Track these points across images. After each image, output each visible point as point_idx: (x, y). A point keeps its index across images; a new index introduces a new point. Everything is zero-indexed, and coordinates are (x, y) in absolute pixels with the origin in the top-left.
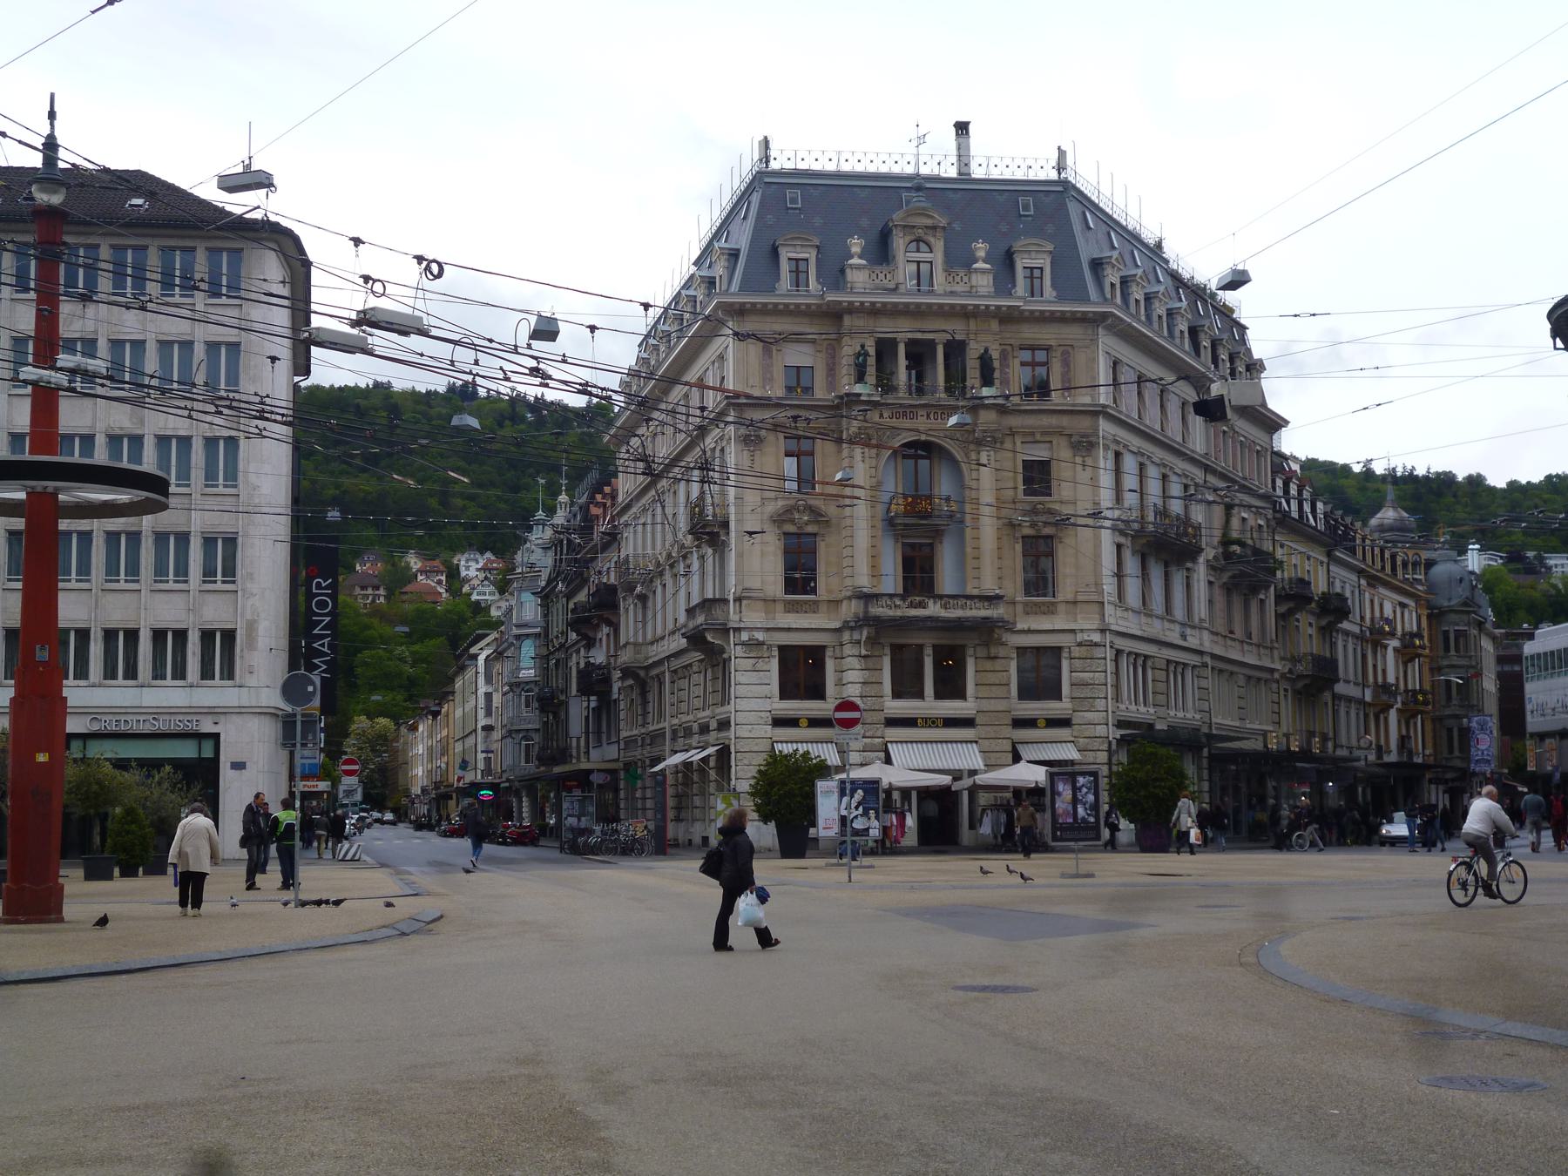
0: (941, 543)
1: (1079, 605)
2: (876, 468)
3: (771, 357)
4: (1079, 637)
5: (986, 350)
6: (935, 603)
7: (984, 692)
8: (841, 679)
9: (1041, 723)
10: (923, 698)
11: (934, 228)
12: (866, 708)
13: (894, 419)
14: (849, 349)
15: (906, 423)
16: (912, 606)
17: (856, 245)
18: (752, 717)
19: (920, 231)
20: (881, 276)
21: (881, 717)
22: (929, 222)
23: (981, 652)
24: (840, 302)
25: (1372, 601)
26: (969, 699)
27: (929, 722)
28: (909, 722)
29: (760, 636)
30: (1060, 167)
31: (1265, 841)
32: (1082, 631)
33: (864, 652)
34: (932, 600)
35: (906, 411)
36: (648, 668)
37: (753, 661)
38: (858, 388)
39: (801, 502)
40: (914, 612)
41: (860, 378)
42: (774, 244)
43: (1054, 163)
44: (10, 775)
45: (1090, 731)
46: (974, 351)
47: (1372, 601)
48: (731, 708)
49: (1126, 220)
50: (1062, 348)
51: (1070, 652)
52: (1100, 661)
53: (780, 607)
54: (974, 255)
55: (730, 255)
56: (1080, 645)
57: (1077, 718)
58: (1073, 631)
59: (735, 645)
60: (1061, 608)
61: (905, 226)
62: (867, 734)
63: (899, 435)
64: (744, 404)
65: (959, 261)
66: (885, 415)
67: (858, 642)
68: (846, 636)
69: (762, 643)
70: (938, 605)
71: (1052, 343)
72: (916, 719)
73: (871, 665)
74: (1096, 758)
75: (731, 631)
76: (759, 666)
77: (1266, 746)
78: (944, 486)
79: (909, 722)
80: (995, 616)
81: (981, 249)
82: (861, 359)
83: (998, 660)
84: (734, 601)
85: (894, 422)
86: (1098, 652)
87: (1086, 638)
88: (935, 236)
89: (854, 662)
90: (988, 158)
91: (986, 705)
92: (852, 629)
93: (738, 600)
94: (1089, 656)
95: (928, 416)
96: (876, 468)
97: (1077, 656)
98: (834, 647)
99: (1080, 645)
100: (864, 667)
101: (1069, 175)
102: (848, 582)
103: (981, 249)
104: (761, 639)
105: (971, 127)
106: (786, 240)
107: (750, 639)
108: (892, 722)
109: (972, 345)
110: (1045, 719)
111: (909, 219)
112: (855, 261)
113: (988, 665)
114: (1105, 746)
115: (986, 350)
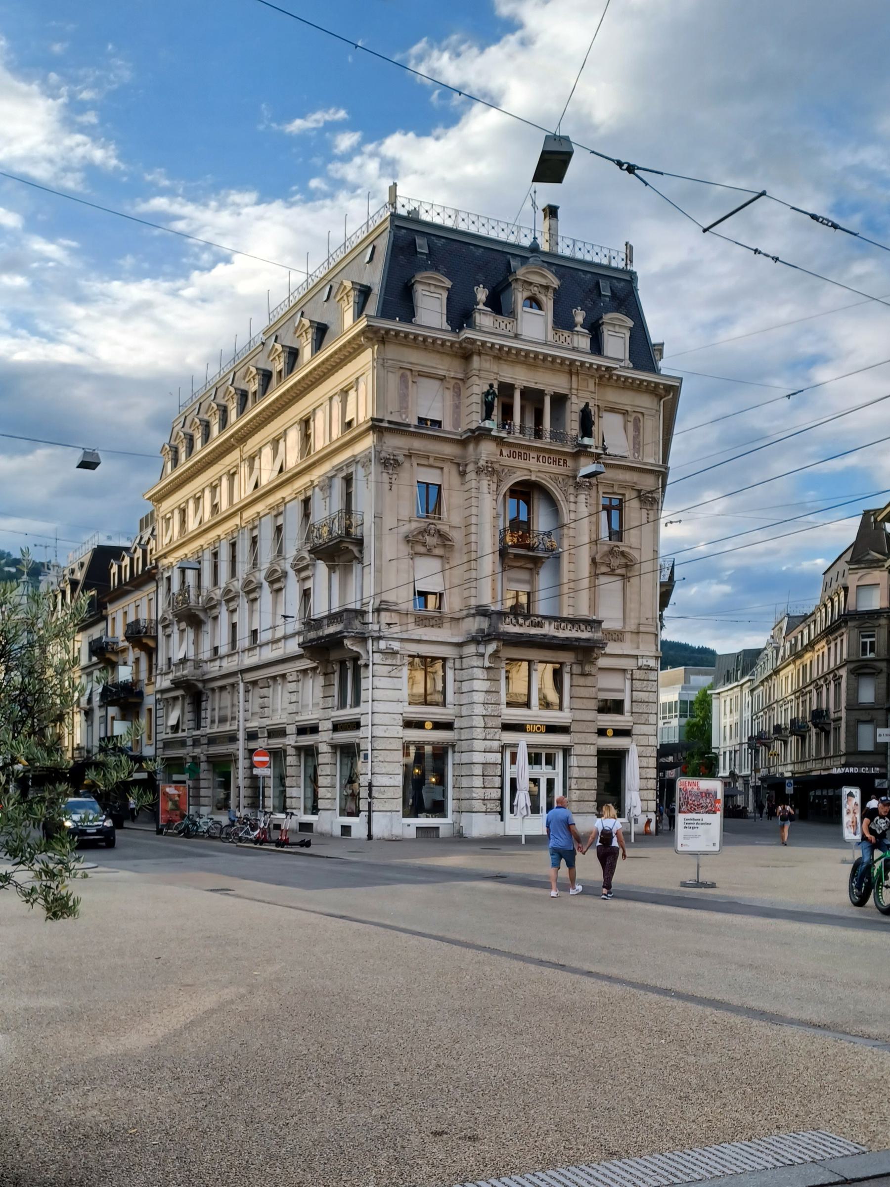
0: (538, 574)
1: (641, 635)
2: (496, 500)
3: (407, 388)
4: (641, 662)
5: (587, 404)
6: (550, 624)
7: (578, 704)
8: (460, 688)
11: (547, 288)
12: (488, 714)
13: (512, 458)
14: (478, 387)
15: (521, 463)
17: (482, 294)
18: (386, 719)
19: (536, 289)
20: (503, 325)
21: (498, 722)
22: (543, 282)
23: (577, 669)
24: (475, 340)
26: (626, 714)
29: (396, 646)
32: (643, 656)
33: (487, 664)
35: (520, 451)
36: (205, 682)
37: (390, 668)
38: (488, 424)
39: (432, 526)
40: (534, 631)
41: (488, 416)
42: (406, 284)
45: (644, 741)
46: (575, 406)
48: (363, 708)
50: (634, 415)
51: (632, 675)
52: (654, 683)
53: (411, 619)
54: (574, 320)
55: (360, 291)
56: (640, 668)
57: (636, 730)
58: (636, 657)
59: (373, 652)
60: (628, 637)
61: (525, 281)
62: (488, 737)
63: (514, 473)
64: (386, 428)
65: (563, 322)
66: (505, 453)
67: (483, 655)
68: (471, 649)
69: (397, 653)
70: (552, 626)
71: (629, 408)
73: (492, 676)
75: (370, 641)
76: (393, 674)
77: (289, 755)
78: (542, 522)
80: (595, 638)
81: (580, 316)
82: (490, 397)
83: (485, 690)
84: (373, 612)
85: (512, 462)
87: (645, 663)
88: (546, 296)
89: (479, 673)
90: (574, 241)
91: (579, 715)
92: (478, 643)
93: (378, 611)
95: (538, 459)
96: (496, 500)
97: (638, 678)
98: (454, 659)
99: (640, 668)
100: (486, 678)
101: (635, 267)
102: (473, 602)
103: (580, 316)
104: (395, 648)
105: (559, 211)
106: (423, 278)
107: (387, 648)
109: (574, 399)
111: (528, 276)
112: (481, 306)
113: (581, 681)
115: (587, 404)
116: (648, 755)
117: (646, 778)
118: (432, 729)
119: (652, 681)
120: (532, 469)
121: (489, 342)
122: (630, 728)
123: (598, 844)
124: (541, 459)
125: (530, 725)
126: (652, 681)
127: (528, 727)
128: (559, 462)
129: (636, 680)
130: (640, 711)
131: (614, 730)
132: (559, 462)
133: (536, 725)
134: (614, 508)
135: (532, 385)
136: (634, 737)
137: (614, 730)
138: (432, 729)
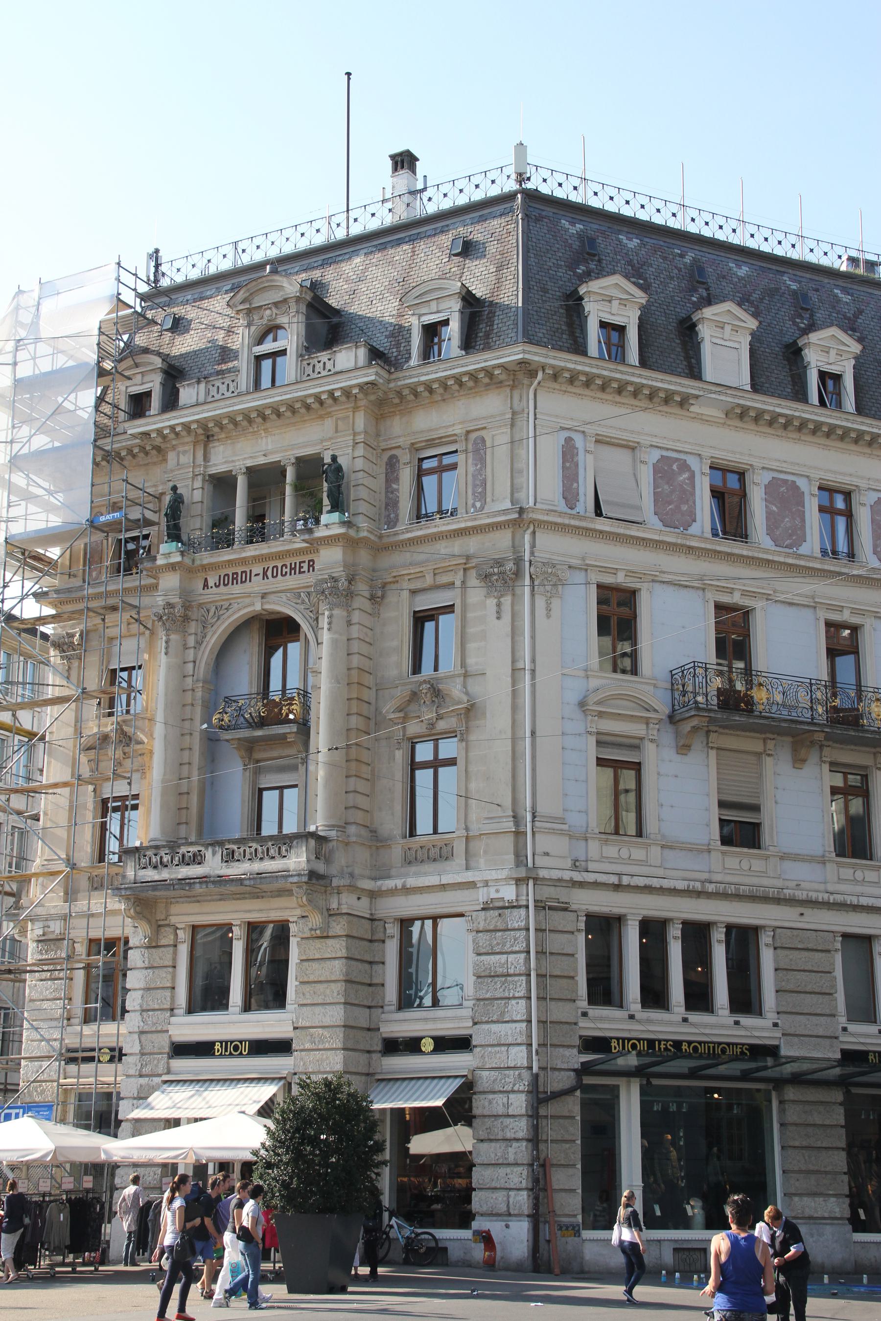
9: (427, 1045)
10: (712, 1012)
16: (185, 861)
25: (12, 849)
27: (231, 1048)
28: (203, 1049)
30: (521, 178)
31: (102, 1207)
32: (486, 884)
34: (210, 849)
43: (511, 170)
44: (791, 1303)
47: (12, 849)
49: (71, 357)
52: (518, 934)
58: (472, 885)
72: (213, 1044)
74: (508, 1105)
79: (203, 1049)
86: (516, 919)
87: (494, 895)
94: (500, 926)
108: (181, 1050)
110: (433, 1038)
114: (524, 1085)
116: (508, 1088)
117: (505, 1140)
118: (421, 1038)
119: (514, 930)
120: (812, 475)
121: (323, 392)
122: (776, 1043)
123: (73, 1198)
124: (269, 573)
125: (618, 1039)
126: (514, 930)
127: (614, 1043)
128: (301, 567)
129: (519, 929)
130: (488, 996)
131: (434, 1038)
132: (301, 567)
133: (629, 1040)
134: (840, 513)
135: (262, 460)
136: (477, 1050)
137: (434, 1038)
138: (421, 1038)
